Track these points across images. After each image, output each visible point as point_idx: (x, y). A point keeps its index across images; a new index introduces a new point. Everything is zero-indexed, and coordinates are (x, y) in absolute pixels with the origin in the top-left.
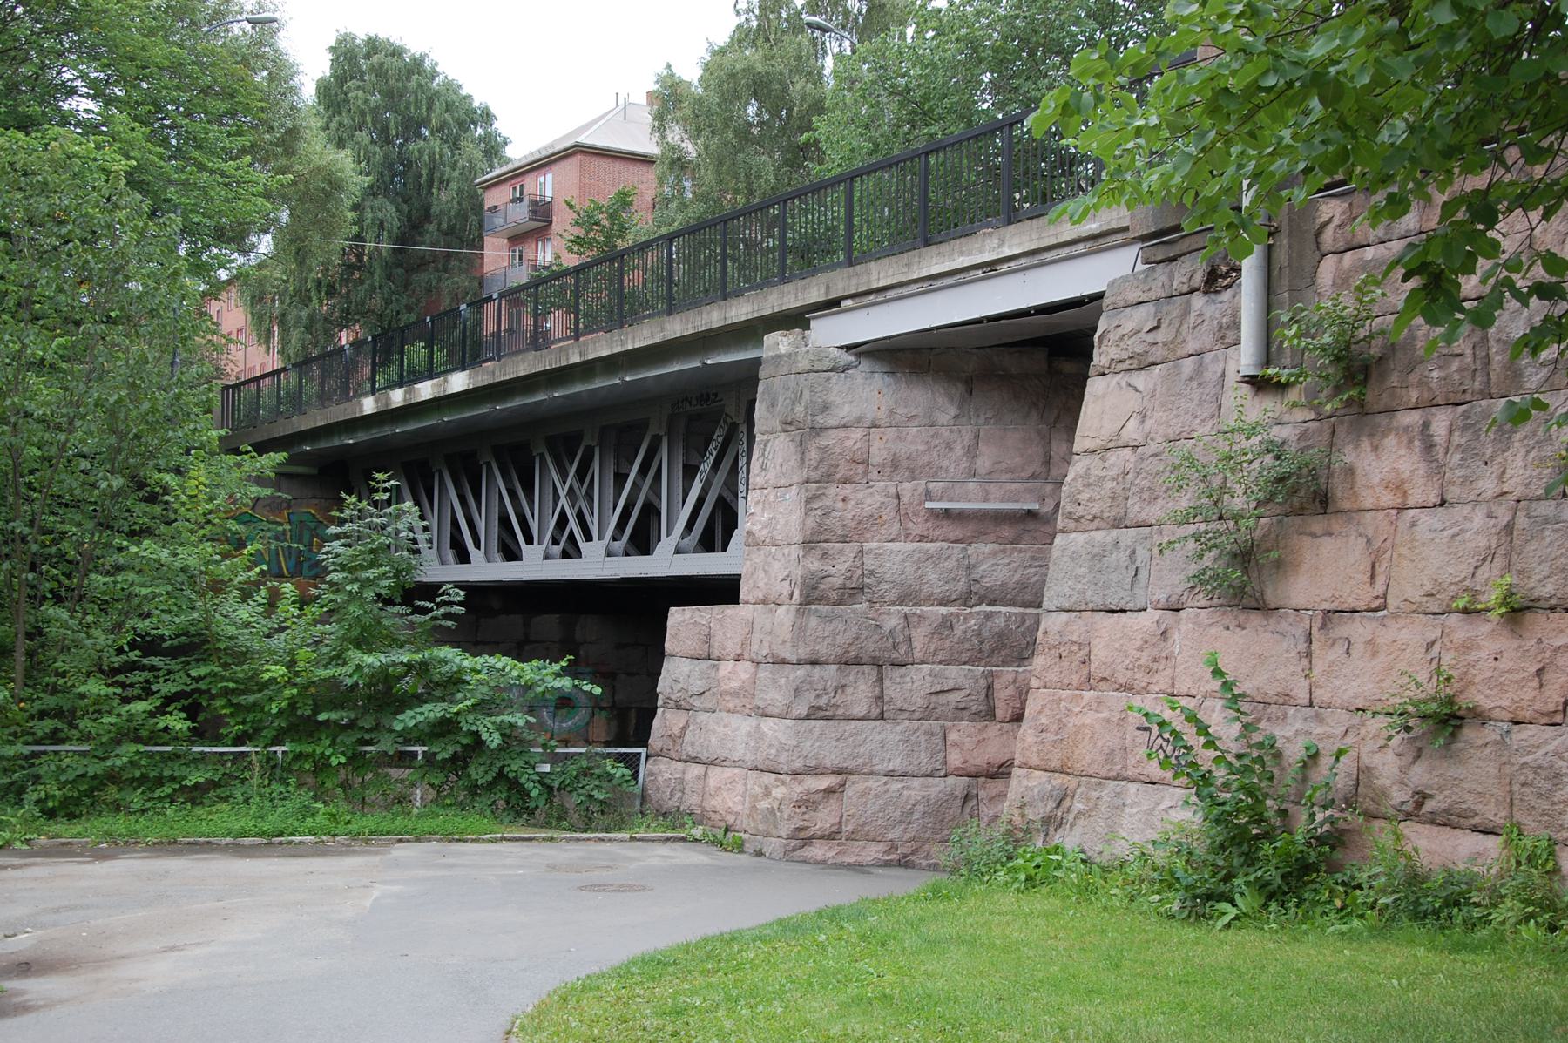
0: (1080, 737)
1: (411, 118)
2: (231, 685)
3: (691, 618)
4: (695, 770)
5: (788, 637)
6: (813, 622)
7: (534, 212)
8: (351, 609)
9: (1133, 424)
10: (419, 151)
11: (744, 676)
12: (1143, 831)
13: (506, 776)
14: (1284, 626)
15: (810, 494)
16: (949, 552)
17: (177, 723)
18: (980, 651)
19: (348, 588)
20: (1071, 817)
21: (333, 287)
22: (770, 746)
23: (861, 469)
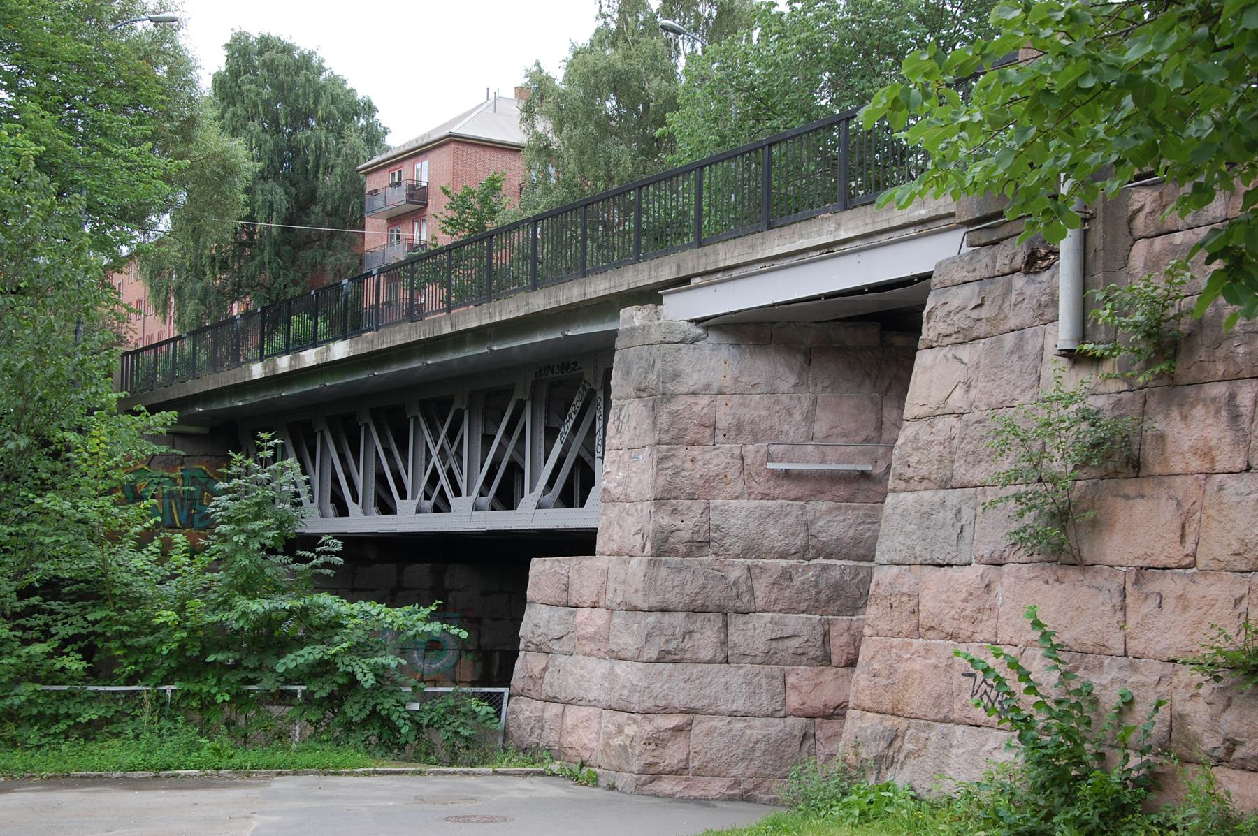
0: (909, 682)
1: (299, 110)
2: (125, 628)
3: (552, 567)
4: (554, 709)
5: (641, 586)
6: (663, 572)
7: (411, 196)
8: (238, 557)
9: (958, 393)
10: (306, 140)
11: (599, 622)
12: (968, 770)
13: (379, 714)
14: (1099, 581)
15: (661, 455)
16: (789, 509)
17: (74, 663)
18: (817, 601)
19: (235, 539)
20: (901, 756)
21: (226, 263)
22: (623, 687)
23: (708, 432)
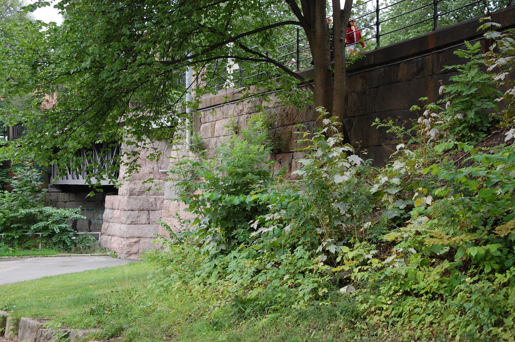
4: (110, 237)
6: (132, 200)
23: (144, 161)
